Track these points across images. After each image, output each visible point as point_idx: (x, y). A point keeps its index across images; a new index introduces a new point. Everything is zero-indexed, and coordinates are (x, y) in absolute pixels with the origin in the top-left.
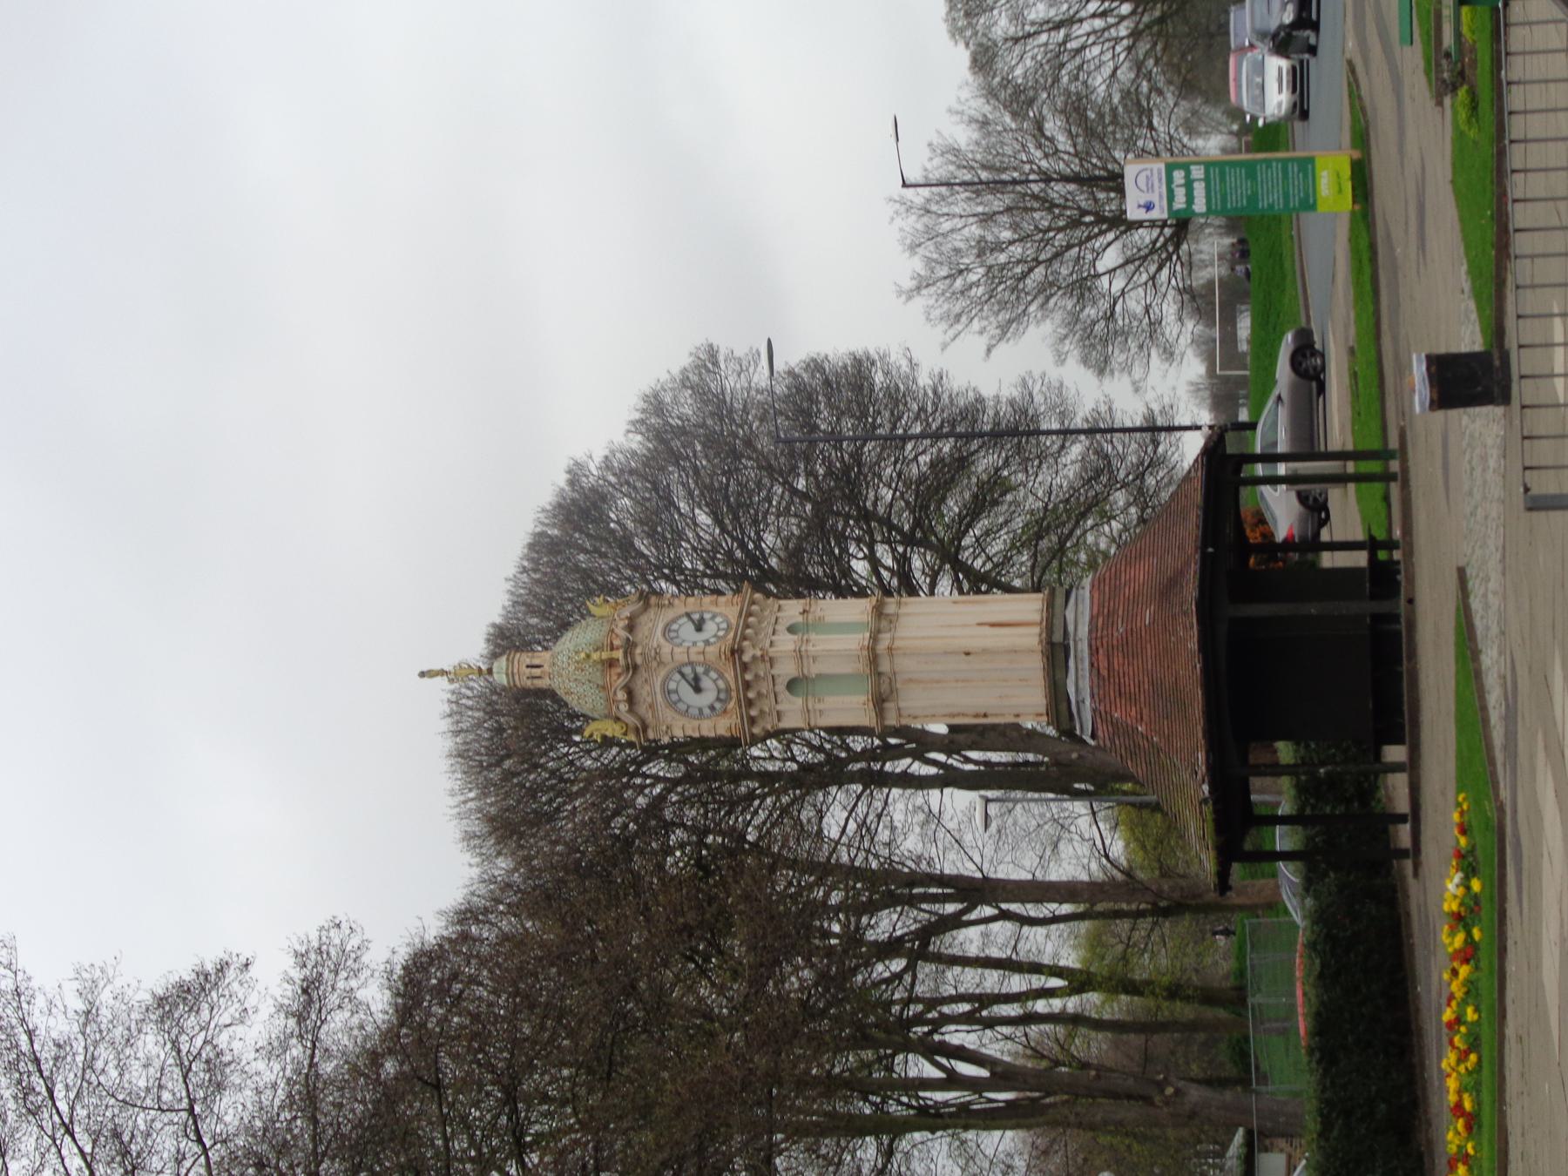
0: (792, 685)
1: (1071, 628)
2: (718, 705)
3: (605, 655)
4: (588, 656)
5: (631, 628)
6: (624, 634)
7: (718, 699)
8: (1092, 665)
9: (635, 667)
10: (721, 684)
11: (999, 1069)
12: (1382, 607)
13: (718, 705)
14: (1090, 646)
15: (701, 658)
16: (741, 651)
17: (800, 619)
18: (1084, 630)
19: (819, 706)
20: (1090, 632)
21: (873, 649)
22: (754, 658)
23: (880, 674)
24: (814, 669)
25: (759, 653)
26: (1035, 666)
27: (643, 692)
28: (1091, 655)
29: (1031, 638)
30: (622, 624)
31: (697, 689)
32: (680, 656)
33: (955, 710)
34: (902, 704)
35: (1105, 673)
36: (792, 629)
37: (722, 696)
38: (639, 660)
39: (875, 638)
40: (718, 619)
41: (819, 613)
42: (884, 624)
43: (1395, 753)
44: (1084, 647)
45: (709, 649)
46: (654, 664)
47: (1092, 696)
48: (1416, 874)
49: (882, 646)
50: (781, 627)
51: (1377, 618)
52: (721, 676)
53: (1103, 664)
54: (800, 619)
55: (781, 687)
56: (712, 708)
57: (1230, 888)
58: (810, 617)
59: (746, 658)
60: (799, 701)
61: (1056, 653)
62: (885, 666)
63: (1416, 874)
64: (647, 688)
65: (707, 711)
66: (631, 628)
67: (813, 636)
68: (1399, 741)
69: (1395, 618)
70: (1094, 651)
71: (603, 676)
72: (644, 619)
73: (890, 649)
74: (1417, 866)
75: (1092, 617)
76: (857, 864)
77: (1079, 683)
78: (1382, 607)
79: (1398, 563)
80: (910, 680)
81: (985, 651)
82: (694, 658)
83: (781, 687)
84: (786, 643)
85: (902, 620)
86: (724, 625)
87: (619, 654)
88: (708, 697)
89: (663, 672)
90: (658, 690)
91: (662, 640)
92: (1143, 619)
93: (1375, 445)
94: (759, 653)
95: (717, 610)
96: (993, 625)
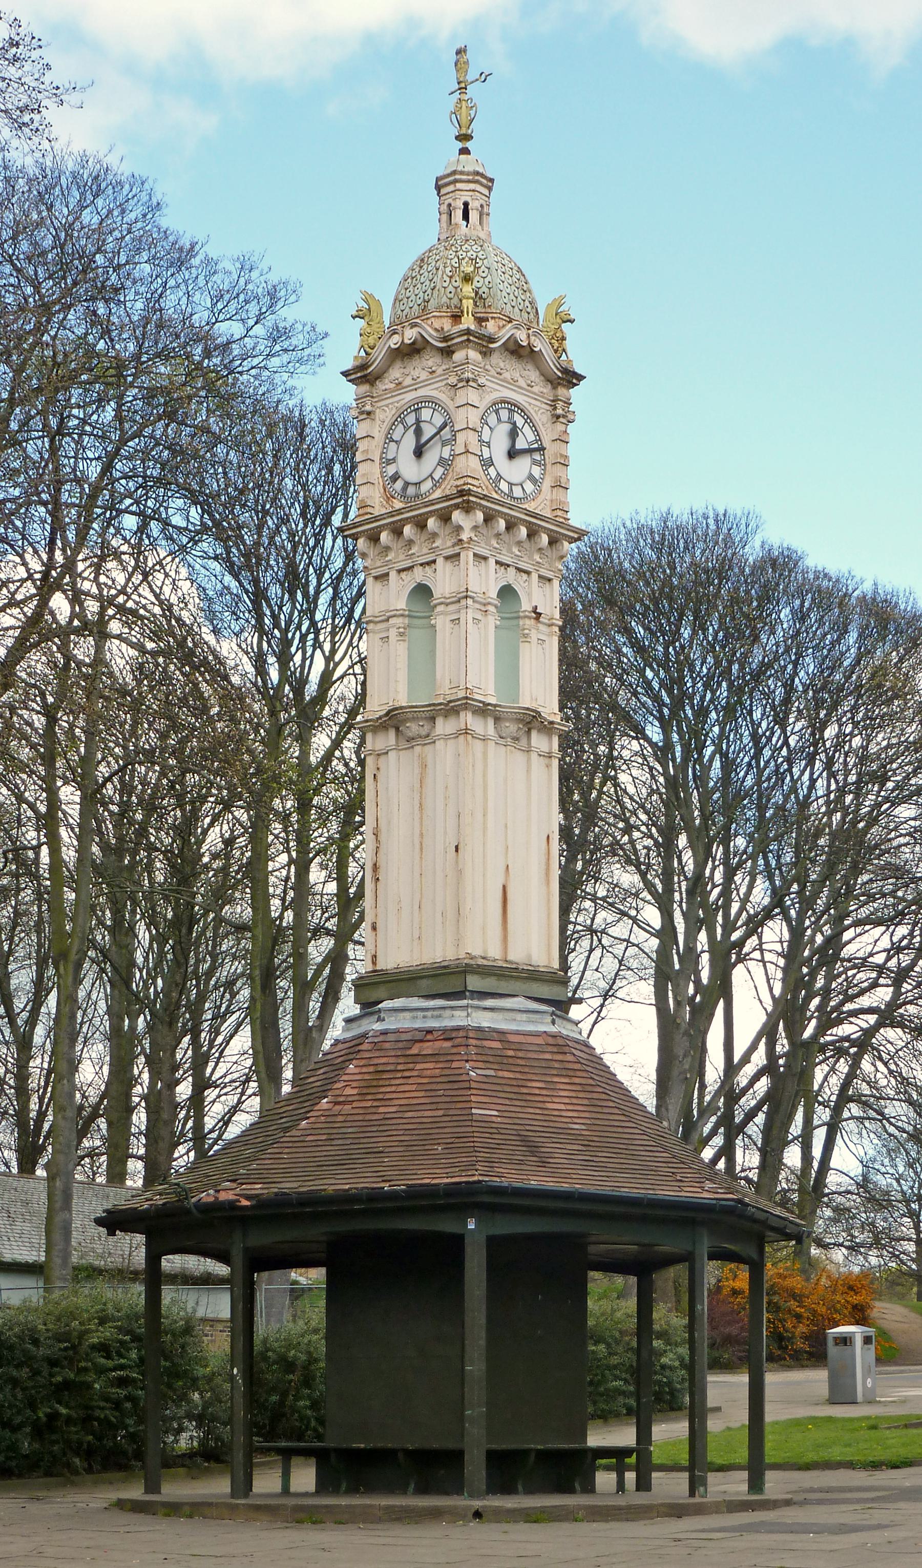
0: (422, 591)
1: (489, 1003)
2: (399, 485)
3: (468, 304)
4: (467, 279)
5: (516, 350)
6: (505, 334)
7: (407, 484)
8: (429, 1032)
9: (447, 352)
10: (427, 486)
11: (315, 1034)
12: (475, 1466)
13: (399, 485)
14: (458, 1029)
15: (460, 449)
16: (468, 508)
17: (526, 606)
18: (485, 1020)
19: (393, 633)
20: (479, 1029)
21: (466, 707)
22: (459, 528)
23: (433, 719)
24: (441, 622)
25: (464, 536)
26: (438, 951)
27: (418, 369)
28: (445, 1030)
29: (482, 943)
30: (521, 336)
31: (419, 453)
32: (465, 417)
33: (382, 838)
34: (392, 755)
35: (414, 1051)
36: (507, 592)
37: (411, 490)
38: (458, 356)
39: (484, 710)
40: (529, 487)
41: (534, 635)
42: (511, 728)
43: (305, 1478)
44: (459, 1019)
45: (473, 463)
46: (453, 380)
47: (385, 1033)
48: (121, 1505)
49: (468, 719)
50: (511, 577)
51: (454, 1458)
52: (437, 485)
53: (428, 1048)
54: (526, 606)
55: (419, 575)
56: (395, 478)
57: (111, 1233)
58: (529, 623)
59: (457, 516)
60: (402, 604)
61: (449, 981)
62: (443, 726)
63: (121, 1505)
64: (424, 375)
65: (391, 470)
66: (516, 350)
67: (492, 621)
68: (324, 1485)
69: (457, 1487)
70: (448, 1034)
71: (438, 308)
72: (533, 375)
73: (466, 731)
74: (137, 1507)
75: (502, 1033)
76: (29, 614)
77: (404, 1015)
78: (475, 1466)
79: (589, 1488)
80: (424, 766)
81: (460, 872)
82: (461, 437)
83: (419, 575)
84: (485, 581)
85: (520, 757)
86: (517, 492)
87: (468, 322)
88: (409, 469)
89: (443, 397)
90: (421, 392)
91: (495, 396)
92: (482, 1105)
93: (771, 1453)
94: (464, 536)
95: (546, 485)
96: (504, 887)
